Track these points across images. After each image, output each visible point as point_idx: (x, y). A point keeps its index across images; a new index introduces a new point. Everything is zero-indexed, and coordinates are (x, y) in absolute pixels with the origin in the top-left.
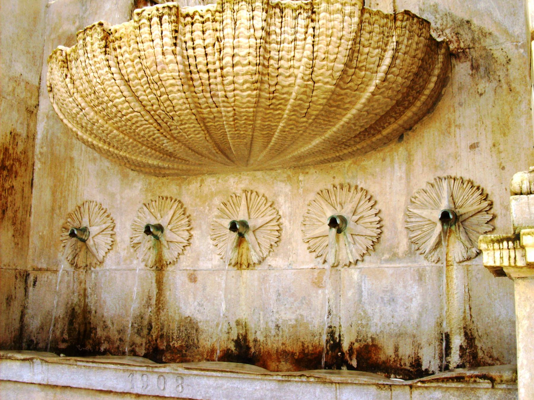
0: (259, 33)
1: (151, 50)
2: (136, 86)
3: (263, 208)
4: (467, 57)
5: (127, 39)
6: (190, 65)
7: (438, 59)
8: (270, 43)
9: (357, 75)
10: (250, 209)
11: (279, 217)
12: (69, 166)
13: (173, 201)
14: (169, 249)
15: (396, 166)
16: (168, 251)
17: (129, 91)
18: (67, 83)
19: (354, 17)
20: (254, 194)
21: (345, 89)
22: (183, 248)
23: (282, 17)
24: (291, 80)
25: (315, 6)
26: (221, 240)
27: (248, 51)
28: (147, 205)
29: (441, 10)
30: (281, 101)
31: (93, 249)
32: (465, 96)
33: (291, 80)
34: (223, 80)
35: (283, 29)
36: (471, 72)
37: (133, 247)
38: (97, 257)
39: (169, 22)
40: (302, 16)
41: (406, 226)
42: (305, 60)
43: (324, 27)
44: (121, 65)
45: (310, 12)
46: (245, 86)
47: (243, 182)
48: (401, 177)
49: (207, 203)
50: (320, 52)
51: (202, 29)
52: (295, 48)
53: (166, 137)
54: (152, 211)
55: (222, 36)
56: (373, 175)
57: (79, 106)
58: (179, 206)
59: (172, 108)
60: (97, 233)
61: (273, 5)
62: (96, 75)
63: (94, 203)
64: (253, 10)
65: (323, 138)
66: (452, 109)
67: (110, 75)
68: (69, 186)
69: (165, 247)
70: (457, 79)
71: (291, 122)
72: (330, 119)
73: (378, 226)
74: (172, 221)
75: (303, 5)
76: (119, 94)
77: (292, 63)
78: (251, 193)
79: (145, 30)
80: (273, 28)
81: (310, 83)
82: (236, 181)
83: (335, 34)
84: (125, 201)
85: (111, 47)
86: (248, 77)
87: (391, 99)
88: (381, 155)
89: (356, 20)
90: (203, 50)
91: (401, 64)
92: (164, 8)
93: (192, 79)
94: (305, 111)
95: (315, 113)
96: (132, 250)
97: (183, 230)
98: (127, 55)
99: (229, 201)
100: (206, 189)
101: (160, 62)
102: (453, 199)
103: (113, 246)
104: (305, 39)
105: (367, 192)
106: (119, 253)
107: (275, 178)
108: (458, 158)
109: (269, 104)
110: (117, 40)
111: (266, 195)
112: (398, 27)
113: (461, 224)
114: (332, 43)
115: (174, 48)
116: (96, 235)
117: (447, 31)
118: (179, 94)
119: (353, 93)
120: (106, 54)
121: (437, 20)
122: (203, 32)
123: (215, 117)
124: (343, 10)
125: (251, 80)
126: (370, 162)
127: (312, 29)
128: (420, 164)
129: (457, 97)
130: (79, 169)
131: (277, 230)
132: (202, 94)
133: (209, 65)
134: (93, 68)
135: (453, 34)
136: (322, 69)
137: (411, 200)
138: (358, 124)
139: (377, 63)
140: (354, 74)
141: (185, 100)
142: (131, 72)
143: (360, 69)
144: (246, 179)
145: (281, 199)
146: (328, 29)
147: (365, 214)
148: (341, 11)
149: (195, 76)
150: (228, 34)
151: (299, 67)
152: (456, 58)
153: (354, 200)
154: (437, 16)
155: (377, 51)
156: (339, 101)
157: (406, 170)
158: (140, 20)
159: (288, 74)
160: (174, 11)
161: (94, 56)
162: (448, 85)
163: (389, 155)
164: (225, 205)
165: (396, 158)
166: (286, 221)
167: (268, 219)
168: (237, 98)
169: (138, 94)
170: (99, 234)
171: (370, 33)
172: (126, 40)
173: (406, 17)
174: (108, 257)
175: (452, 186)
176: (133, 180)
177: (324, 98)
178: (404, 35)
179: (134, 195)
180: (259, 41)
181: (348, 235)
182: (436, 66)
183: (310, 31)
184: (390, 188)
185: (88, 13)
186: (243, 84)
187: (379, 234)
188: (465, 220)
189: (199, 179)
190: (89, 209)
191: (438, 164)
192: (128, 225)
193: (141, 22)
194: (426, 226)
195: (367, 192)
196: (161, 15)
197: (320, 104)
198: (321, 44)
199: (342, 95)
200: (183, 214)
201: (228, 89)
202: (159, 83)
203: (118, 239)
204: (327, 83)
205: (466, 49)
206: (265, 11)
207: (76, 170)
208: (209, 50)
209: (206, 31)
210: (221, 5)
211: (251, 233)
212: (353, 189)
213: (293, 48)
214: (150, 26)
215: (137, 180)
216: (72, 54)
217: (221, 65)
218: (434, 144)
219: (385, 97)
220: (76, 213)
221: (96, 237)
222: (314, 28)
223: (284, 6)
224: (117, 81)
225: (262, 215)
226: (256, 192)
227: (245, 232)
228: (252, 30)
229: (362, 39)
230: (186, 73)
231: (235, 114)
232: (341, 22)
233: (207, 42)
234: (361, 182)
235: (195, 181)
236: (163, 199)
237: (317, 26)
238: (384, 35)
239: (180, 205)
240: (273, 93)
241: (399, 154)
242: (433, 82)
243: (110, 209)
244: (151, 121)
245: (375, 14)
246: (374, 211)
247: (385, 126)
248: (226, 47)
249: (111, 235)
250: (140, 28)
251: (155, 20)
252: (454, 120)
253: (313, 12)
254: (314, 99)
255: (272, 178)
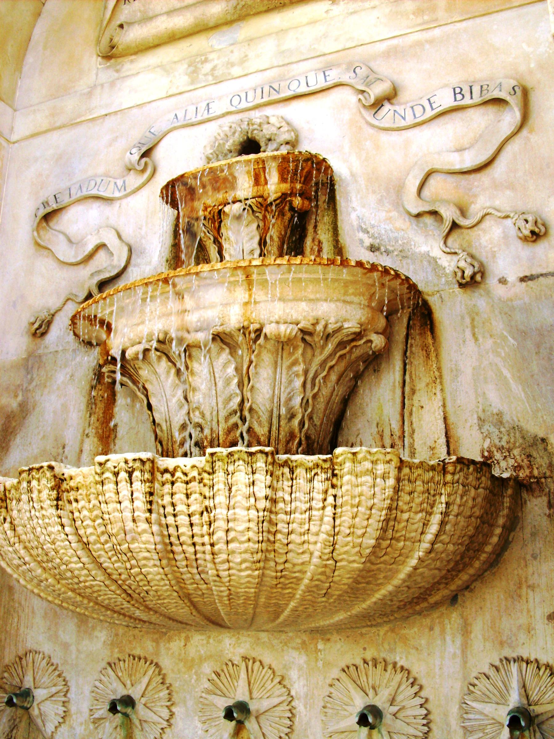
0: (262, 504)
1: (117, 514)
2: (98, 551)
3: (269, 685)
4: (543, 491)
5: (85, 491)
6: (169, 536)
7: (503, 503)
8: (277, 513)
9: (393, 546)
10: (251, 685)
11: (291, 699)
12: (7, 599)
13: (148, 663)
14: (142, 730)
15: (448, 638)
16: (140, 733)
17: (88, 557)
18: (6, 529)
19: (389, 478)
20: (257, 664)
21: (377, 564)
22: (161, 731)
23: (292, 479)
24: (306, 557)
25: (336, 467)
26: (213, 724)
27: (247, 525)
28: (113, 665)
29: (507, 422)
30: (291, 580)
31: (39, 721)
32: (541, 545)
33: (306, 557)
34: (214, 558)
35: (293, 496)
36: (547, 512)
37: (94, 722)
38: (44, 733)
39: (141, 481)
40: (320, 478)
41: (462, 724)
42: (323, 536)
43: (348, 495)
44: (78, 523)
45: (330, 472)
46: (244, 566)
47: (242, 645)
48: (455, 654)
49: (194, 671)
50: (344, 526)
51: (185, 492)
52: (310, 519)
53: (138, 608)
54: (120, 674)
55: (212, 505)
56: (417, 649)
57: (22, 560)
58: (157, 672)
59: (146, 583)
60: (43, 699)
61: (280, 462)
62: (44, 531)
63: (41, 654)
64: (253, 473)
65: (349, 613)
66: (522, 563)
67: (63, 536)
68: (6, 625)
69: (137, 727)
70: (529, 521)
71: (305, 603)
72: (358, 595)
73: (425, 722)
74: (146, 692)
75: (321, 462)
76: (76, 559)
77: (306, 537)
78: (254, 662)
79: (110, 487)
80: (280, 494)
81: (331, 562)
82: (233, 643)
83: (363, 503)
84: (83, 656)
85: (65, 498)
86: (247, 556)
87: (439, 570)
88: (427, 621)
89: (391, 482)
90: (187, 518)
91: (453, 530)
92: (135, 460)
93: (173, 552)
94: (324, 591)
95: (337, 593)
96: (92, 726)
97: (162, 706)
98: (85, 513)
99: (223, 671)
100: (192, 651)
101: (130, 531)
102: (525, 691)
103: (66, 718)
104: (323, 508)
105: (409, 673)
106: (74, 729)
107: (286, 644)
108: (532, 632)
109: (276, 583)
110: (73, 489)
111: (273, 666)
112: (448, 483)
113: (537, 729)
114: (359, 514)
115: (148, 515)
116: (43, 701)
117: (516, 452)
118: (156, 569)
119: (388, 567)
120: (57, 509)
121: (502, 436)
122: (188, 496)
123: (203, 594)
124: (374, 471)
125: (252, 559)
126: (412, 631)
127: (333, 498)
128: (480, 637)
129: (529, 545)
130: (20, 603)
131: (289, 718)
132: (186, 569)
133: (195, 538)
134: (40, 521)
135: (523, 456)
136: (346, 546)
137: (468, 688)
138: (395, 599)
139: (420, 530)
140: (390, 546)
141: (164, 577)
142: (91, 534)
143: (398, 540)
144: (246, 641)
145: (294, 674)
146: (353, 497)
147: (407, 703)
148: (371, 472)
149: (177, 549)
150: (220, 503)
151: (316, 543)
152: (527, 491)
153: (392, 684)
154: (502, 429)
155: (420, 515)
156: (370, 577)
157: (462, 645)
158: (103, 473)
159: (301, 551)
160: (148, 466)
161: (42, 508)
162: (518, 529)
163: (439, 623)
164: (218, 675)
165: (449, 626)
166: (301, 704)
167: (276, 701)
168: (232, 578)
169: (102, 560)
170: (46, 699)
171: (410, 493)
172: (84, 493)
173: (458, 468)
174: (59, 733)
175: (524, 673)
176: (94, 628)
177: (349, 578)
178: (456, 493)
179: (94, 649)
180: (261, 514)
181: (384, 733)
182: (501, 513)
183: (330, 500)
184: (440, 668)
185: (34, 384)
186: (241, 563)
187: (426, 733)
188: (543, 723)
189: (183, 635)
190: (33, 662)
191: (505, 639)
192: (87, 689)
193: (105, 476)
194: (489, 727)
195: (409, 673)
196: (130, 470)
197: (344, 584)
198: (344, 516)
199: (373, 571)
200: (162, 683)
201: (221, 568)
202: (129, 554)
203: (73, 708)
204: (354, 561)
205: (541, 478)
206: (269, 474)
207: (17, 605)
208: (196, 519)
209: (191, 494)
210: (211, 464)
211: (253, 719)
212: (390, 667)
213: (307, 520)
214: (117, 483)
215: (99, 628)
216: (13, 491)
217: (212, 541)
218: (499, 611)
219: (431, 570)
220: (15, 665)
221: (42, 704)
222: (335, 496)
223: (294, 464)
224: (72, 545)
225: (268, 695)
226: (261, 662)
227: (245, 719)
228: (252, 500)
229: (400, 503)
230: (165, 544)
231: (230, 594)
232: (371, 487)
233: (192, 509)
234: (401, 658)
235: (177, 638)
236: (134, 659)
237: (339, 494)
238: (429, 494)
239: (157, 670)
240: (282, 571)
241: (452, 623)
242: (496, 535)
243: (62, 665)
244: (118, 592)
245: (417, 468)
246: (418, 701)
247: (433, 593)
248: (218, 519)
249: (64, 702)
250: (103, 483)
251: (123, 475)
252: (526, 578)
253: (334, 475)
254: (335, 579)
255: (281, 643)
